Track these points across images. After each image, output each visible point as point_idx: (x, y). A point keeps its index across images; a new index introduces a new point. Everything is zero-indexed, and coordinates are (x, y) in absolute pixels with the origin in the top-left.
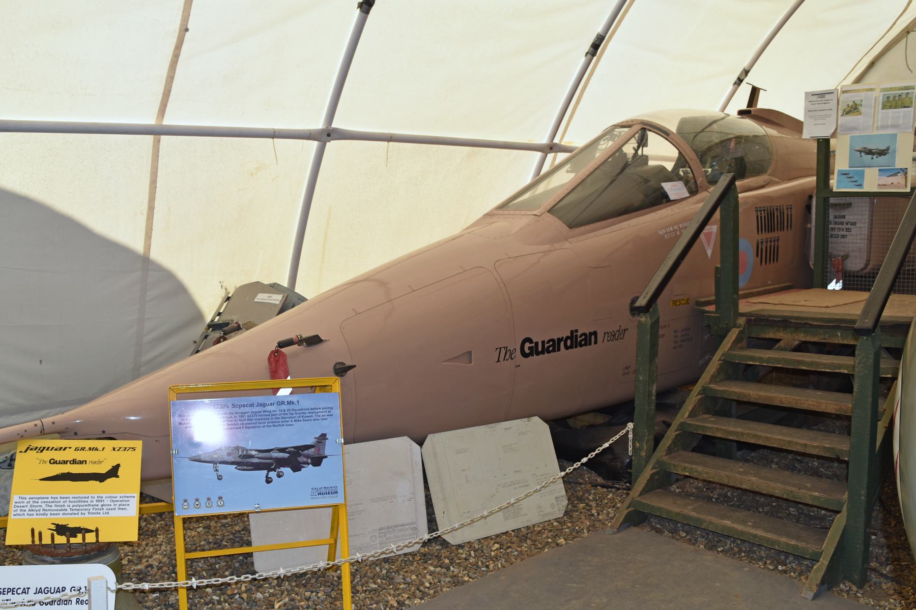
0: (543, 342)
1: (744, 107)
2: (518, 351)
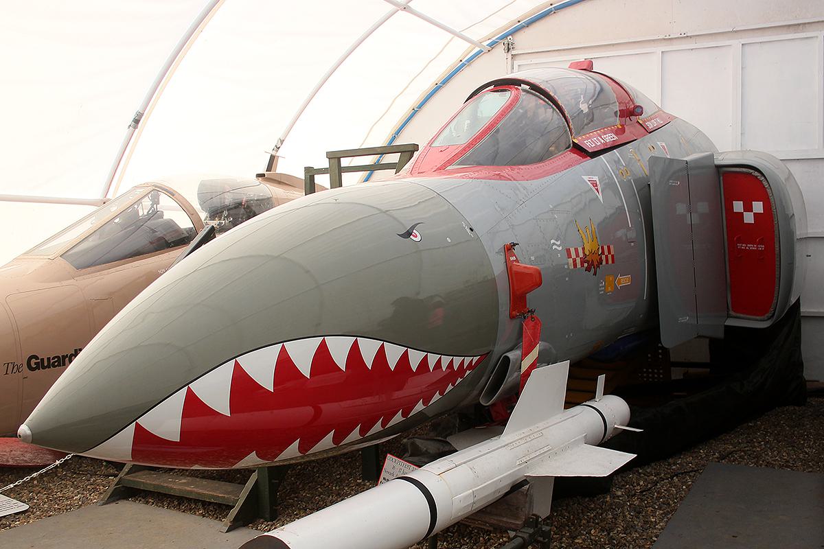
0: (49, 359)
1: (262, 170)
2: (25, 365)
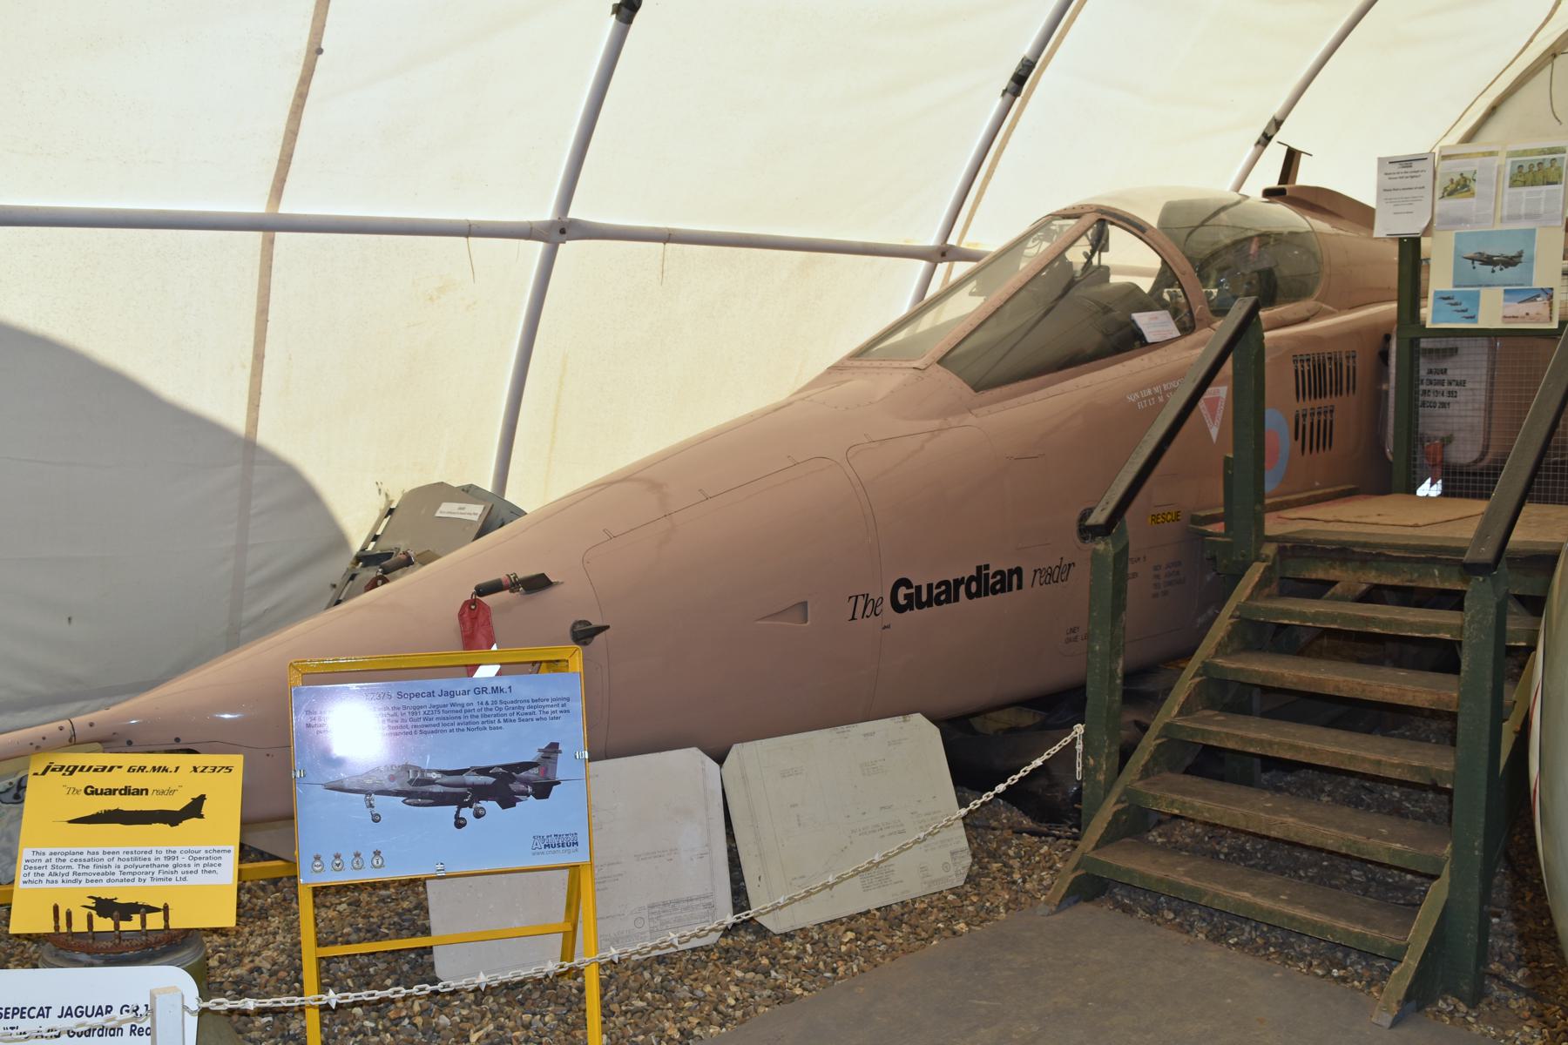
0: (930, 586)
1: (1273, 183)
2: (887, 601)
